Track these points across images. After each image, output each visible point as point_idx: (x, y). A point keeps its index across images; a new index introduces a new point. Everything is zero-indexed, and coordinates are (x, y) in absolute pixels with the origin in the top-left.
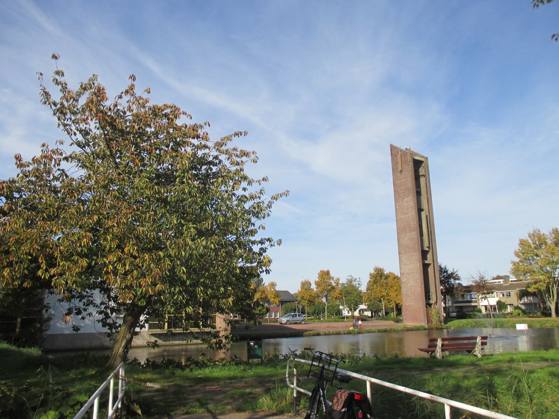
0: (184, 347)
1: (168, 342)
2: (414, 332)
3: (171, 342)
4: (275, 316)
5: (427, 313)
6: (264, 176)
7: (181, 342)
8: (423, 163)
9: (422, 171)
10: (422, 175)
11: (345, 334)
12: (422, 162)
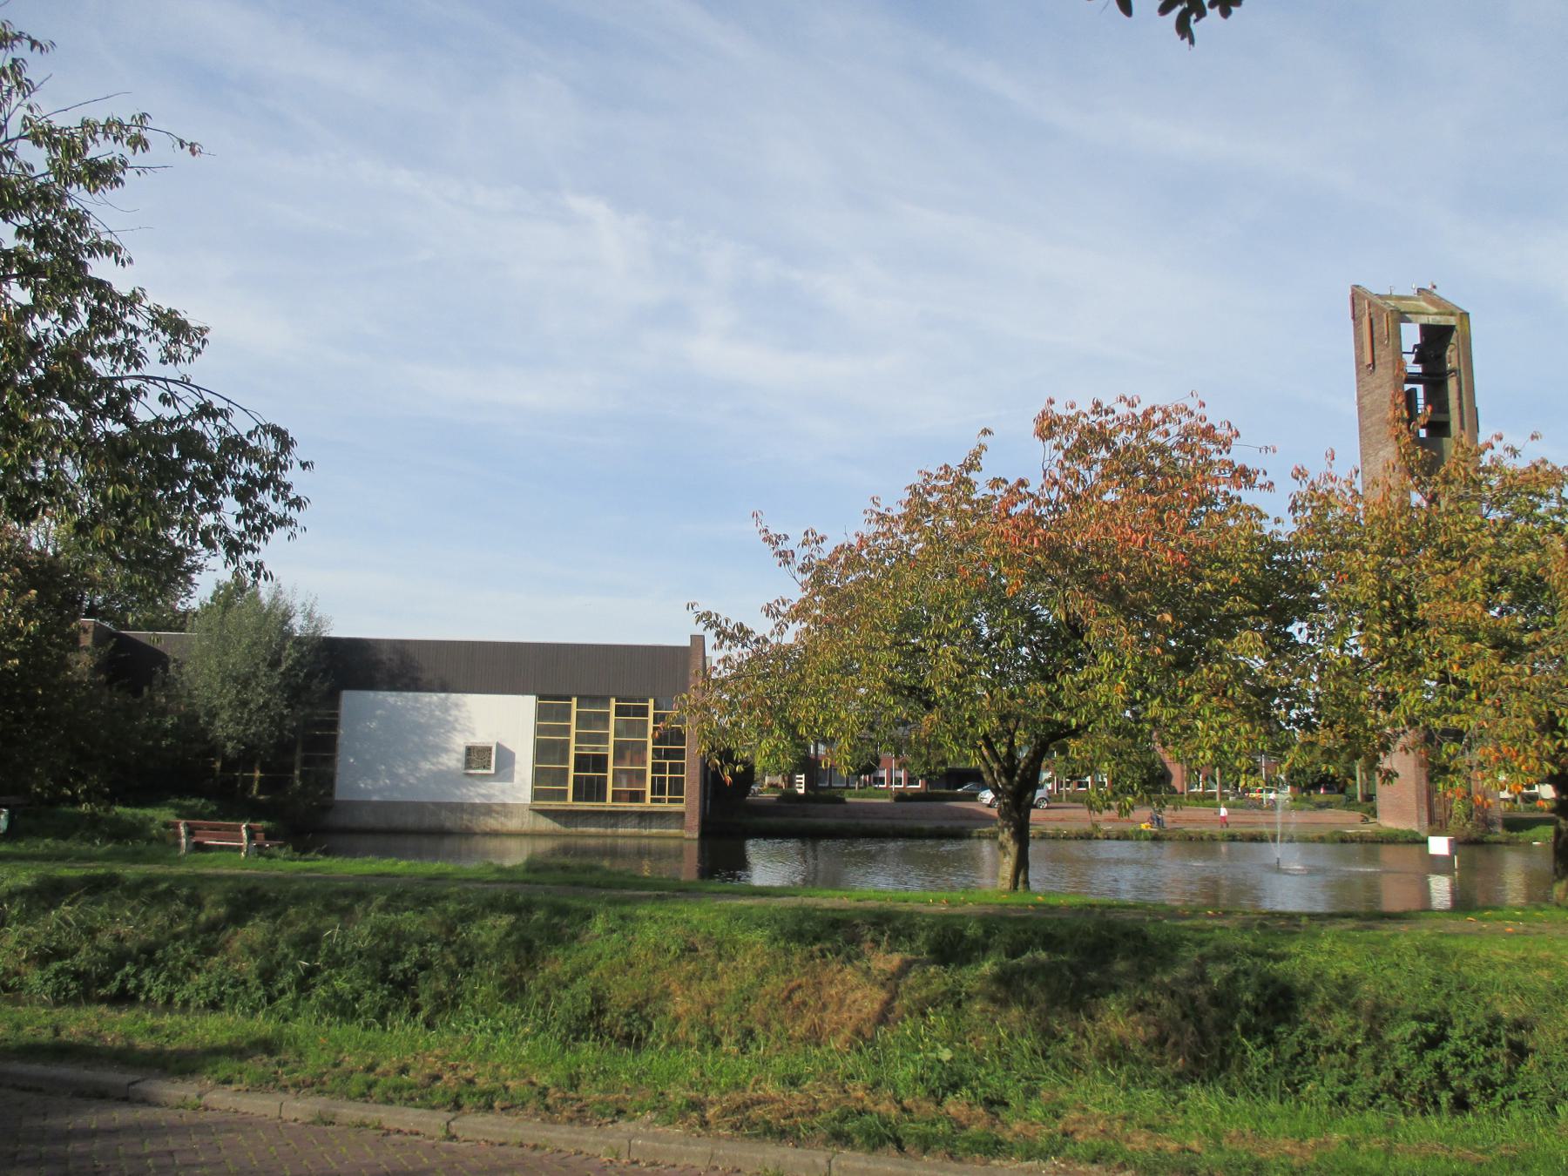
0: (609, 841)
1: (573, 830)
2: (1400, 847)
3: (580, 829)
4: (13, 655)
5: (1431, 794)
6: (1047, 398)
7: (601, 830)
8: (1455, 334)
9: (1452, 358)
10: (1451, 371)
11: (1108, 838)
12: (1449, 330)
